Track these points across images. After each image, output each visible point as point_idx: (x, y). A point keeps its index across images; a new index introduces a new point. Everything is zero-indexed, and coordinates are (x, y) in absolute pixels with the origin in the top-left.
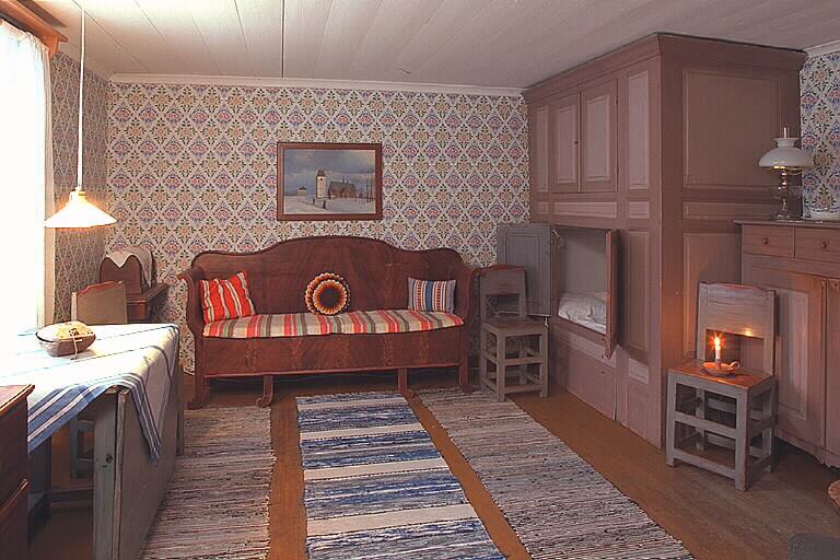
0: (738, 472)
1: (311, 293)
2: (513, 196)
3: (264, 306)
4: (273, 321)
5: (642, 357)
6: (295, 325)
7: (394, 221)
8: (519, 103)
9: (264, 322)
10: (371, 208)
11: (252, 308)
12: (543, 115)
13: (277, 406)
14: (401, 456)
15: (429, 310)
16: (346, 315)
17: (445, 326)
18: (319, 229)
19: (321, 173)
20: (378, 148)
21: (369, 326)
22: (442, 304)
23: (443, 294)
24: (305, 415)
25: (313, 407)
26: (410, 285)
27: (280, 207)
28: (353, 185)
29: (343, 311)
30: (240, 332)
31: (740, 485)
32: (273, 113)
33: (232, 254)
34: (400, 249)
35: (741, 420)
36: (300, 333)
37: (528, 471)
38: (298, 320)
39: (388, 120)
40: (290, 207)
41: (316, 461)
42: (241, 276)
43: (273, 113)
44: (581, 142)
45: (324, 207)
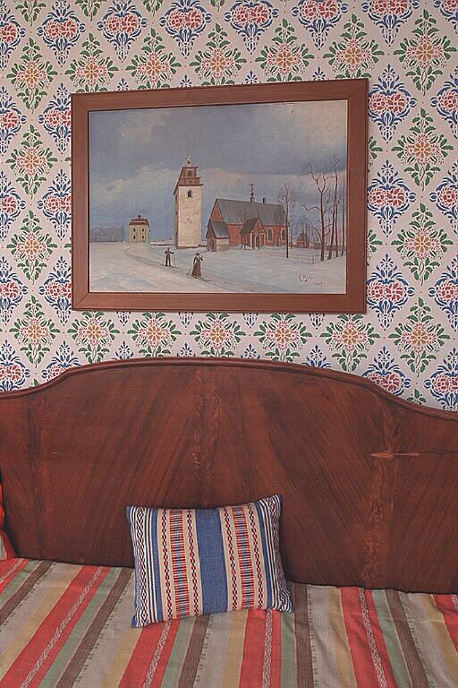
10: (331, 277)
19: (189, 178)
40: (110, 271)
45: (196, 272)
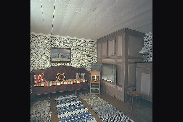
2: (83, 58)
3: (48, 79)
4: (50, 83)
5: (120, 86)
6: (55, 83)
7: (73, 63)
9: (48, 83)
10: (69, 60)
11: (45, 80)
12: (99, 45)
13: (51, 100)
14: (79, 109)
15: (80, 78)
16: (65, 80)
18: (59, 64)
19: (59, 54)
21: (70, 82)
23: (83, 75)
24: (58, 101)
28: (66, 56)
29: (64, 80)
30: (43, 85)
32: (54, 42)
33: (40, 69)
34: (74, 68)
38: (55, 82)
39: (72, 44)
40: (53, 60)
42: (43, 74)
43: (54, 42)
45: (60, 60)
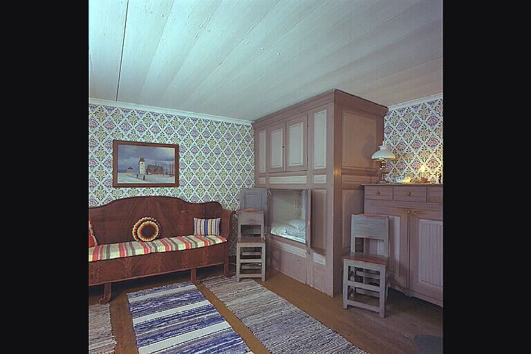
0: (380, 309)
1: (136, 230)
6: (127, 249)
8: (250, 128)
9: (105, 251)
10: (172, 180)
11: (95, 240)
12: (263, 135)
13: (114, 302)
14: (203, 324)
15: (206, 234)
16: (158, 241)
17: (217, 243)
18: (141, 192)
19: (142, 160)
20: (176, 147)
22: (213, 231)
24: (137, 304)
25: (141, 298)
26: (195, 222)
27: (115, 179)
29: (156, 239)
31: (382, 315)
34: (188, 202)
35: (382, 283)
36: (130, 254)
37: (275, 321)
39: (182, 131)
40: (122, 179)
41: (146, 339)
44: (285, 147)
45: (144, 179)
